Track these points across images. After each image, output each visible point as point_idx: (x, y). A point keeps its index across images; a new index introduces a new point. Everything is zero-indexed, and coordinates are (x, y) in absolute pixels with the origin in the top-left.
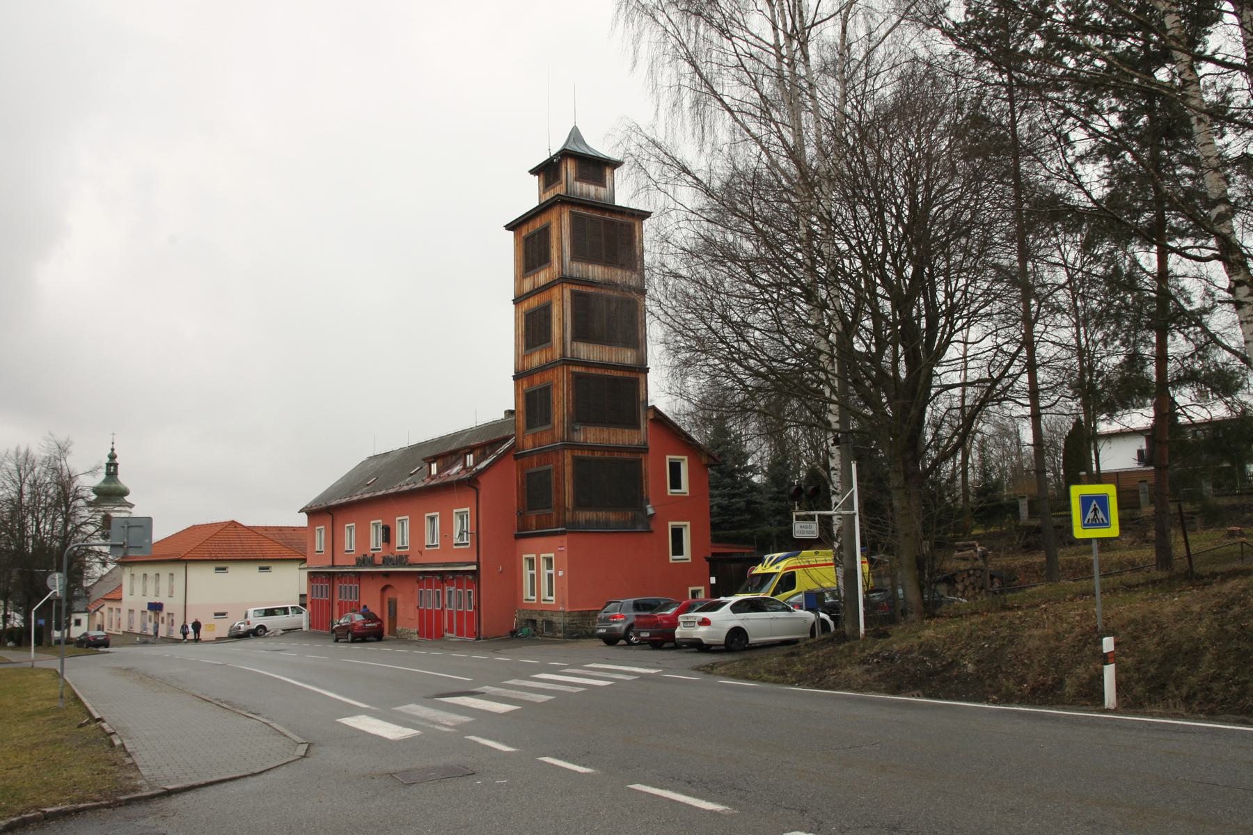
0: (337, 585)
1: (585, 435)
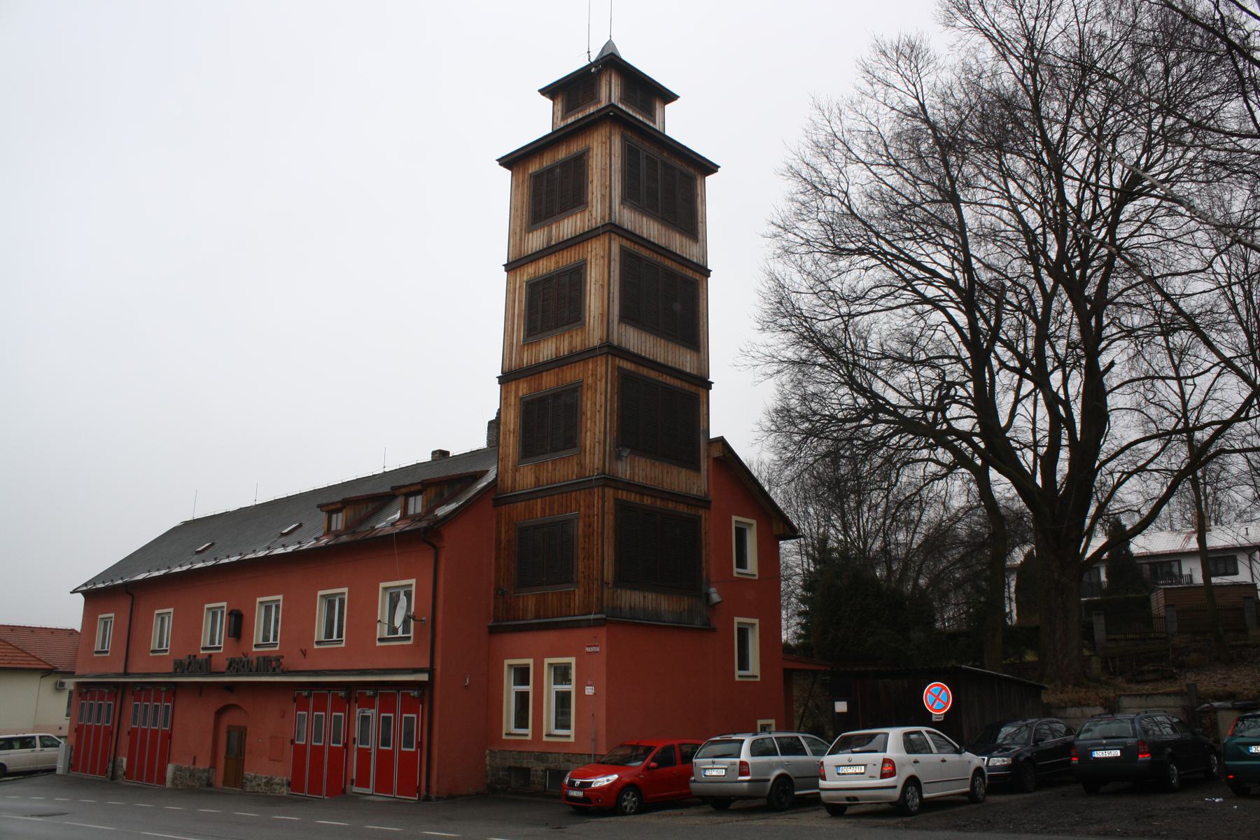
0: (131, 703)
1: (632, 469)
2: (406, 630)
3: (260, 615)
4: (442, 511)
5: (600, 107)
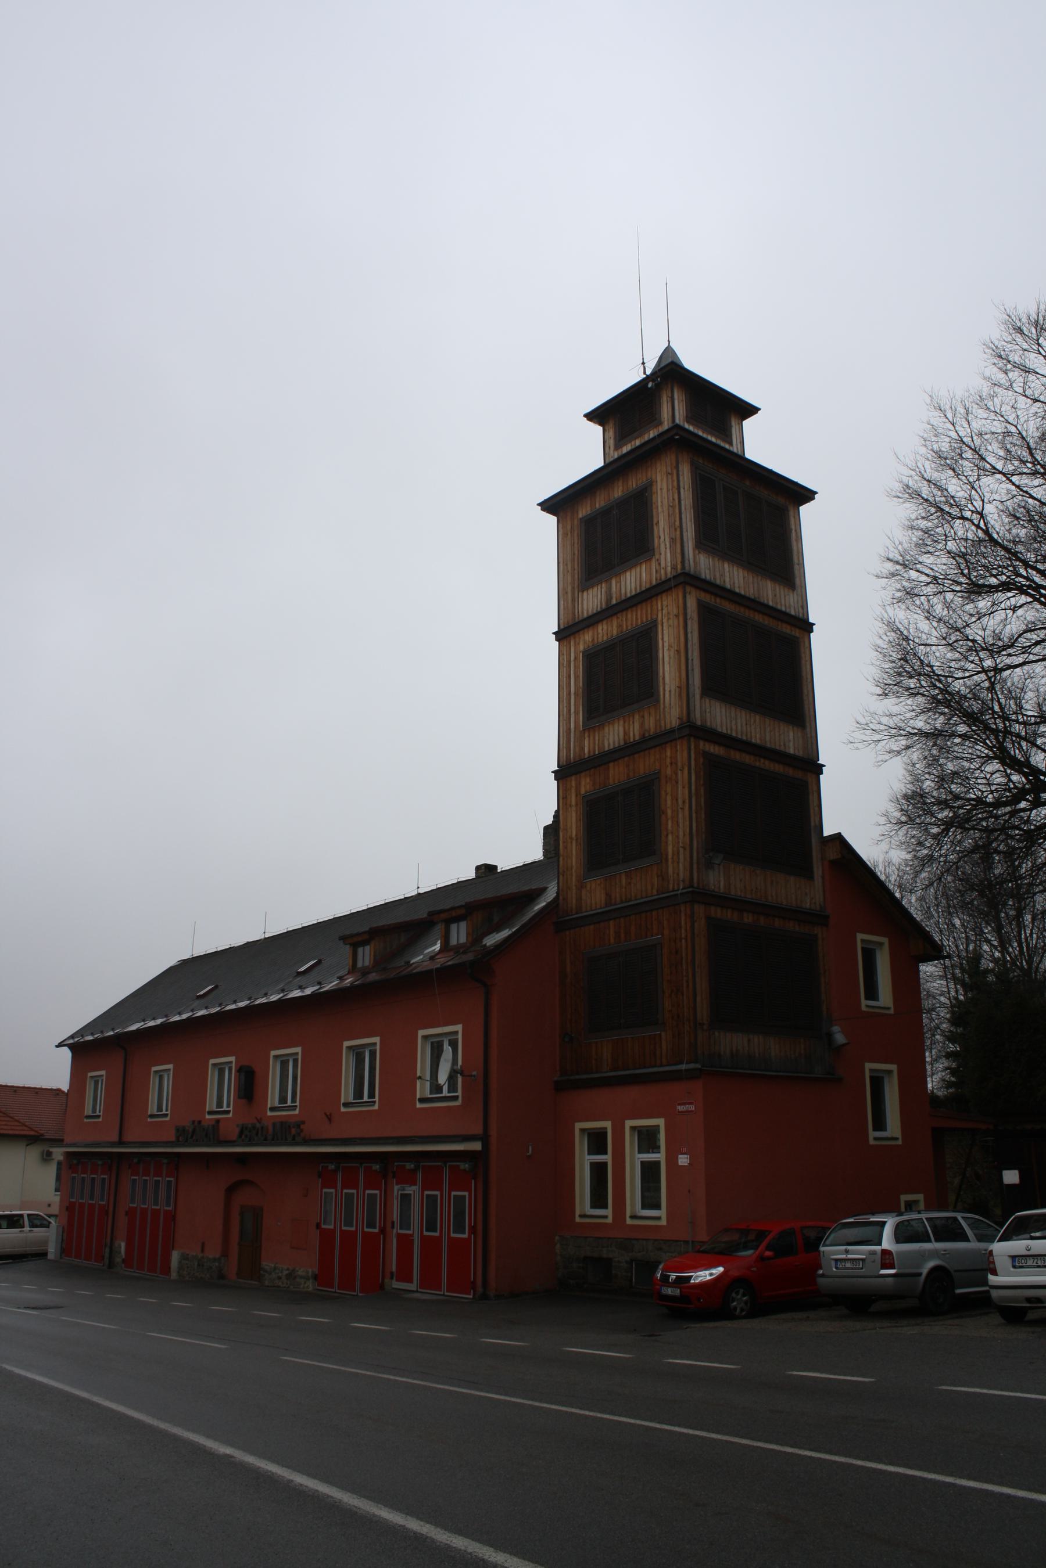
2: (452, 1087)
3: (274, 1072)
4: (492, 940)
5: (661, 429)
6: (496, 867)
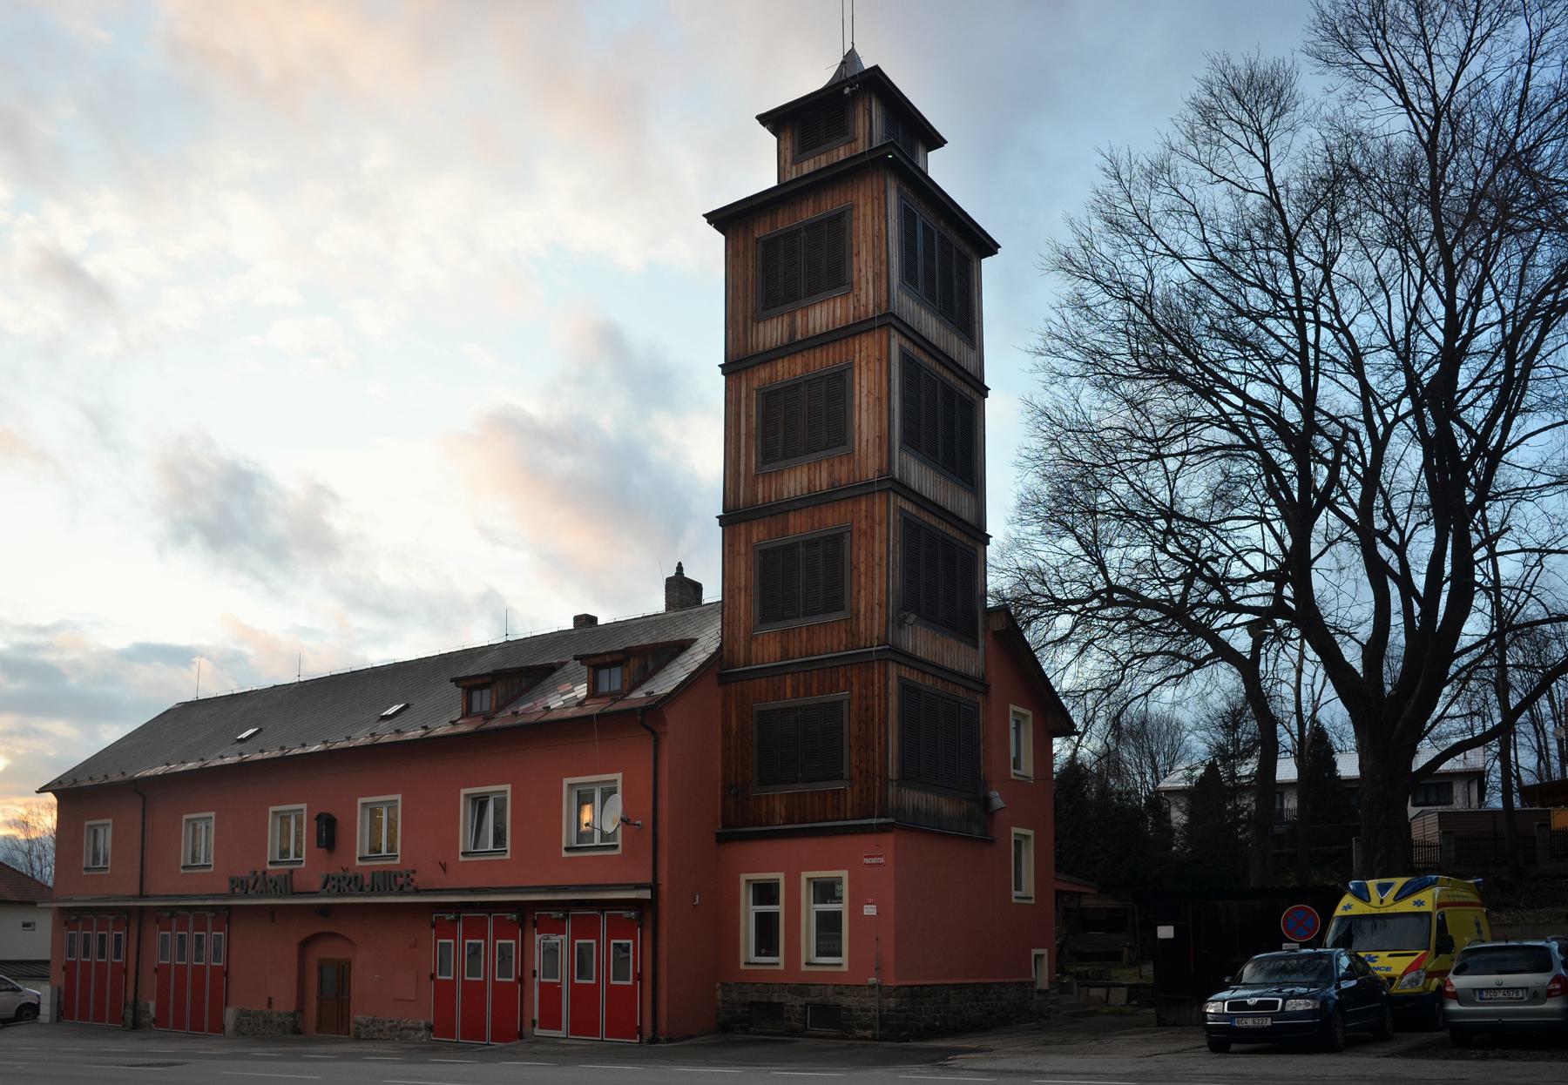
6: (595, 619)
